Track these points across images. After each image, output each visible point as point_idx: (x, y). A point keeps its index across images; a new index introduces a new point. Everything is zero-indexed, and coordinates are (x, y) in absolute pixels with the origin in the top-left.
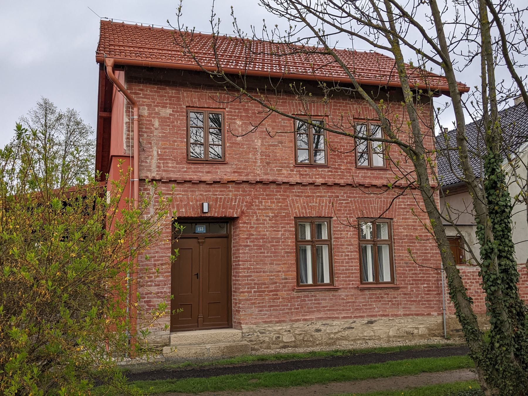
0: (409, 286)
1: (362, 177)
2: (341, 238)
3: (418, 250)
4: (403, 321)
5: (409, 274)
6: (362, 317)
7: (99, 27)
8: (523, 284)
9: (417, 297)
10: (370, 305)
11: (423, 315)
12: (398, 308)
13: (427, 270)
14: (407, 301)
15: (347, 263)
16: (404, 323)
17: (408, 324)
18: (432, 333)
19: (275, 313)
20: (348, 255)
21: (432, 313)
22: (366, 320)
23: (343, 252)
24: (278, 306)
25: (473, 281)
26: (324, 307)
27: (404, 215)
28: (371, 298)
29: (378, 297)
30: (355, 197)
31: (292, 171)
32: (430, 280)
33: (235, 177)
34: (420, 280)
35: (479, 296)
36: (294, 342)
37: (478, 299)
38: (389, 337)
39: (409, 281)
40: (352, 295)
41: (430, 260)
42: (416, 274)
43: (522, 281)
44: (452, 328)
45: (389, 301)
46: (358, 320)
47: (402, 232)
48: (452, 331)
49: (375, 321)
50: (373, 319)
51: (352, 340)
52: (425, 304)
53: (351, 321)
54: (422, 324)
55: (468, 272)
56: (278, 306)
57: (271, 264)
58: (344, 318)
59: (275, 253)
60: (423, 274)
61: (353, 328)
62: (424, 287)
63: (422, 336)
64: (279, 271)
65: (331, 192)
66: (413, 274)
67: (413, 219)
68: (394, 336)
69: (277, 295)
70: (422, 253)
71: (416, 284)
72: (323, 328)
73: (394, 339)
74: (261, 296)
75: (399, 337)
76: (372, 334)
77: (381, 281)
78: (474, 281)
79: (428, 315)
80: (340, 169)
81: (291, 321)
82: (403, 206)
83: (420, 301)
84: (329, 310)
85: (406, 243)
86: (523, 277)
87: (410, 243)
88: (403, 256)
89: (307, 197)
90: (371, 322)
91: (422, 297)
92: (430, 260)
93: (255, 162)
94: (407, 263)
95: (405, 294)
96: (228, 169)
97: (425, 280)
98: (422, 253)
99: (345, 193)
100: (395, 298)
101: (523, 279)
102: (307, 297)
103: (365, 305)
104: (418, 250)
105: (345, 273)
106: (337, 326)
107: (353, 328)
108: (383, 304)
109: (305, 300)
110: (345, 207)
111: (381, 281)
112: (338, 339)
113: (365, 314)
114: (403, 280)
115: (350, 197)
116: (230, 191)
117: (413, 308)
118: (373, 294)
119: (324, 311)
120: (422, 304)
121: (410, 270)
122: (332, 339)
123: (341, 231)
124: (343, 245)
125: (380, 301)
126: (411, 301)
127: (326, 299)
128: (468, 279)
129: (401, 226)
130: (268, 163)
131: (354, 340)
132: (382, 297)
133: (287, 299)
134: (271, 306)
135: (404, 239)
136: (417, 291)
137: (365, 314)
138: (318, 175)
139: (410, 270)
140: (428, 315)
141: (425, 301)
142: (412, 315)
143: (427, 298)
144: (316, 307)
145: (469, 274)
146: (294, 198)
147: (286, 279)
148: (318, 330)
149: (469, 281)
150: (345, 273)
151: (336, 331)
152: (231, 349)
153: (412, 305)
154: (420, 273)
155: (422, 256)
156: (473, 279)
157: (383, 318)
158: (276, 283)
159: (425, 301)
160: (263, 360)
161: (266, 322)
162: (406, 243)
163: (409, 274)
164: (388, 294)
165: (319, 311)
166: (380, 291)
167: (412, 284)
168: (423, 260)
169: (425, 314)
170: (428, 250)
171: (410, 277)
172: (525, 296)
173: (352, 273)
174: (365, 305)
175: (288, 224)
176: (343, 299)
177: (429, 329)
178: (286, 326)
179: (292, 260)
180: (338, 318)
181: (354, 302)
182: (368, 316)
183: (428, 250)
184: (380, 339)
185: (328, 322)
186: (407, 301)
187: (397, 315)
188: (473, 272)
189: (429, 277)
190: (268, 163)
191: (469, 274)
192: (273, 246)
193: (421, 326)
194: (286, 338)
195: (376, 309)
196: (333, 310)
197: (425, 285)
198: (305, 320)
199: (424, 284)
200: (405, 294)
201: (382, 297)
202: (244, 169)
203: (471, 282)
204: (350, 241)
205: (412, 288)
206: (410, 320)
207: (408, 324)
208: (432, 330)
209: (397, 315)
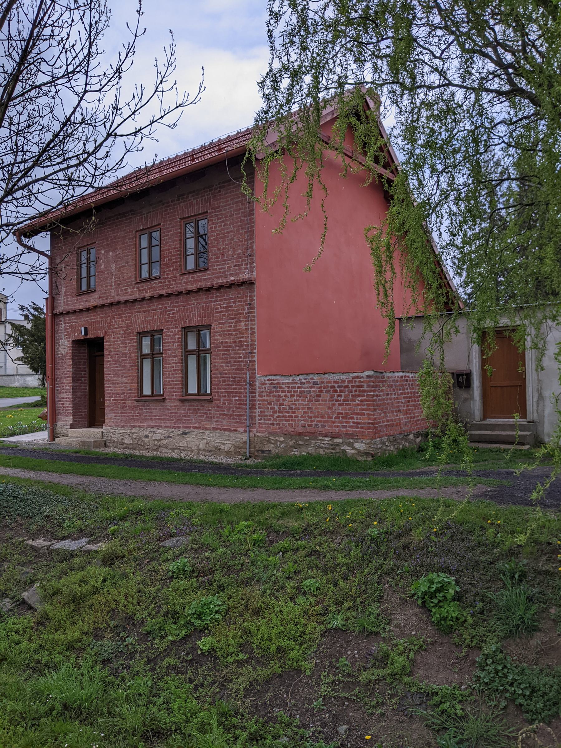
0: (222, 399)
1: (184, 283)
2: (168, 350)
3: (231, 358)
4: (211, 435)
5: (222, 385)
6: (179, 427)
7: (124, 175)
8: (354, 401)
9: (229, 410)
10: (189, 416)
11: (229, 430)
12: (211, 421)
13: (239, 381)
14: (220, 414)
15: (173, 374)
16: (213, 437)
17: (217, 439)
18: (237, 450)
19: (124, 419)
20: (173, 367)
21: (238, 429)
22: (181, 431)
23: (170, 364)
24: (125, 413)
25: (287, 394)
26: (155, 416)
27: (220, 319)
28: (189, 409)
29: (195, 409)
30: (179, 306)
31: (134, 288)
32: (241, 393)
33: (100, 302)
34: (232, 392)
35: (294, 413)
36: (132, 444)
37: (292, 417)
38: (199, 450)
39: (222, 393)
40: (175, 406)
41: (243, 369)
42: (228, 385)
43: (353, 396)
44: (257, 449)
45: (204, 413)
46: (176, 430)
47: (218, 339)
48: (258, 451)
49: (189, 432)
50: (187, 430)
51: (171, 449)
52: (236, 419)
53: (170, 430)
54: (229, 440)
55: (283, 384)
56: (125, 413)
57: (122, 376)
58: (166, 427)
59: (124, 366)
60: (236, 385)
61: (171, 437)
62: (236, 400)
63: (228, 453)
64: (126, 383)
65: (162, 304)
66: (226, 385)
67: (229, 323)
68: (204, 450)
69: (124, 403)
70: (235, 362)
71: (229, 396)
72: (150, 435)
73: (203, 453)
74: (116, 404)
75: (208, 451)
76: (186, 445)
77: (202, 393)
78: (289, 394)
79: (234, 430)
80: (168, 278)
81: (131, 426)
82: (220, 310)
83: (231, 415)
84: (158, 419)
85: (221, 351)
86: (354, 390)
87: (225, 351)
88: (217, 366)
89: (145, 311)
90: (185, 433)
91: (233, 411)
92: (243, 369)
93: (111, 286)
94: (220, 374)
95: (218, 407)
96: (96, 296)
97: (236, 392)
98: (235, 362)
99: (172, 303)
100: (209, 410)
101: (353, 393)
102: (144, 406)
103: (185, 416)
104: (231, 358)
105: (171, 385)
106: (160, 433)
107: (171, 437)
108: (199, 416)
109: (142, 409)
110: (172, 317)
111: (202, 393)
112: (160, 446)
113: (181, 425)
114: (217, 392)
115: (175, 307)
116: (98, 315)
117: (225, 422)
118: (191, 406)
119: (155, 419)
120: (233, 419)
121: (223, 381)
122: (156, 445)
123: (168, 343)
124: (169, 357)
125: (197, 413)
126: (224, 415)
127: (156, 409)
128: (282, 392)
129: (217, 332)
130: (119, 285)
131: (173, 449)
132: (199, 409)
133: (131, 407)
134: (122, 413)
135: (220, 347)
136: (229, 404)
137: (181, 425)
138: (151, 288)
139: (223, 381)
140: (234, 430)
141: (236, 415)
142: (220, 429)
143: (238, 412)
144: (149, 416)
145: (283, 386)
146: (136, 314)
147: (131, 390)
148: (147, 437)
149: (283, 394)
150: (171, 385)
151: (158, 438)
152: (83, 443)
153: (224, 419)
154: (233, 385)
155: (235, 365)
156: (288, 392)
157: (195, 430)
158: (124, 393)
159: (236, 415)
160: (77, 452)
161: (117, 426)
162: (221, 351)
163: (222, 385)
164: (203, 406)
165: (151, 419)
166: (197, 403)
167: (225, 396)
168: (236, 369)
169: (233, 429)
170: (241, 357)
171: (223, 389)
172: (355, 417)
173: (176, 385)
174: (185, 416)
175: (132, 339)
176: (168, 409)
177: (236, 447)
178: (127, 431)
179: (134, 373)
180: (161, 427)
181: (176, 413)
182: (184, 427)
183: (241, 357)
184: (191, 451)
185: (154, 430)
186: (220, 414)
187: (206, 429)
188: (288, 383)
189: (241, 389)
190: (119, 285)
191: (283, 386)
192: (123, 360)
193: (228, 442)
194: (127, 441)
195: (194, 421)
196: (161, 419)
197: (237, 398)
198: (139, 426)
199: (235, 396)
200: (218, 407)
201: (199, 409)
202: (105, 293)
203: (285, 396)
204: (175, 353)
205: (224, 400)
206: (217, 434)
207: (217, 439)
208: (238, 447)
209: (206, 429)
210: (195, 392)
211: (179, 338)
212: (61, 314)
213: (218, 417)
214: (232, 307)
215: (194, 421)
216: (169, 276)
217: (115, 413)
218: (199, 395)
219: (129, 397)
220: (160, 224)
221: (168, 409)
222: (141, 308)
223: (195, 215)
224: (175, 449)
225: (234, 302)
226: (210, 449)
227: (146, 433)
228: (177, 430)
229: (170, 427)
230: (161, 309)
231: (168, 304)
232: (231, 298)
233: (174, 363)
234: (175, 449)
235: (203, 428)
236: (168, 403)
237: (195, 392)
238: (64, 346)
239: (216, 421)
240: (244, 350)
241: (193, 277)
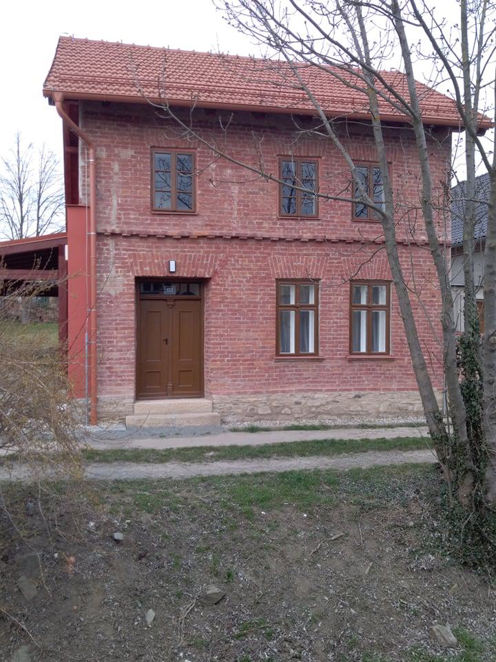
3: (420, 317)
4: (395, 396)
20: (336, 323)
22: (353, 394)
26: (306, 378)
29: (369, 370)
38: (379, 412)
40: (340, 367)
45: (382, 374)
53: (336, 393)
68: (385, 412)
72: (303, 401)
75: (390, 413)
102: (288, 367)
118: (363, 366)
125: (371, 374)
126: (408, 375)
132: (374, 370)
137: (352, 388)
138: (305, 229)
146: (277, 256)
157: (374, 392)
164: (381, 366)
166: (371, 363)
174: (353, 378)
176: (328, 370)
179: (272, 327)
181: (340, 374)
182: (356, 389)
184: (368, 414)
190: (246, 215)
195: (366, 382)
201: (374, 370)
210: (384, 351)
211: (346, 291)
212: (113, 235)
213: (400, 377)
214: (421, 266)
215: (366, 382)
216: (335, 220)
217: (232, 377)
218: (297, 356)
219: (261, 356)
220: (320, 157)
221: (328, 370)
222: (286, 250)
223: (177, 148)
224: (343, 414)
225: (424, 262)
226: (393, 411)
227: (295, 400)
228: (346, 393)
229: (335, 390)
230: (318, 255)
231: (332, 252)
232: (420, 257)
233: (337, 318)
234: (343, 414)
235: (384, 389)
236: (328, 364)
237: (384, 351)
238: (118, 284)
239: (399, 382)
240: (435, 310)
241: (371, 227)
